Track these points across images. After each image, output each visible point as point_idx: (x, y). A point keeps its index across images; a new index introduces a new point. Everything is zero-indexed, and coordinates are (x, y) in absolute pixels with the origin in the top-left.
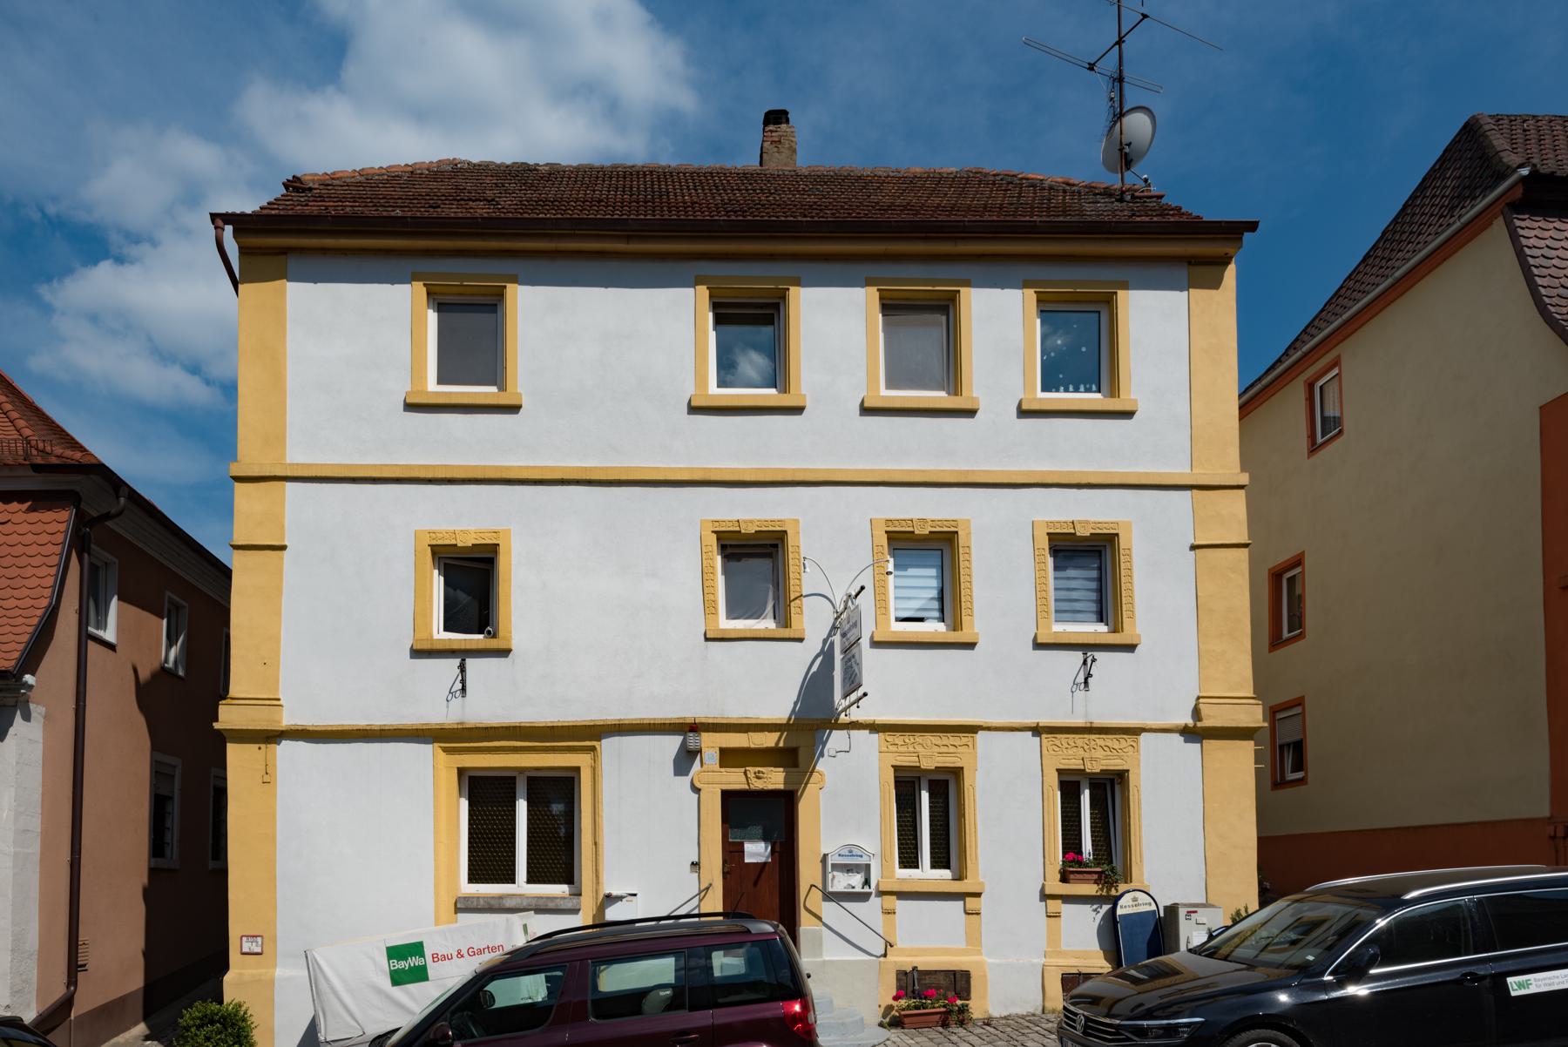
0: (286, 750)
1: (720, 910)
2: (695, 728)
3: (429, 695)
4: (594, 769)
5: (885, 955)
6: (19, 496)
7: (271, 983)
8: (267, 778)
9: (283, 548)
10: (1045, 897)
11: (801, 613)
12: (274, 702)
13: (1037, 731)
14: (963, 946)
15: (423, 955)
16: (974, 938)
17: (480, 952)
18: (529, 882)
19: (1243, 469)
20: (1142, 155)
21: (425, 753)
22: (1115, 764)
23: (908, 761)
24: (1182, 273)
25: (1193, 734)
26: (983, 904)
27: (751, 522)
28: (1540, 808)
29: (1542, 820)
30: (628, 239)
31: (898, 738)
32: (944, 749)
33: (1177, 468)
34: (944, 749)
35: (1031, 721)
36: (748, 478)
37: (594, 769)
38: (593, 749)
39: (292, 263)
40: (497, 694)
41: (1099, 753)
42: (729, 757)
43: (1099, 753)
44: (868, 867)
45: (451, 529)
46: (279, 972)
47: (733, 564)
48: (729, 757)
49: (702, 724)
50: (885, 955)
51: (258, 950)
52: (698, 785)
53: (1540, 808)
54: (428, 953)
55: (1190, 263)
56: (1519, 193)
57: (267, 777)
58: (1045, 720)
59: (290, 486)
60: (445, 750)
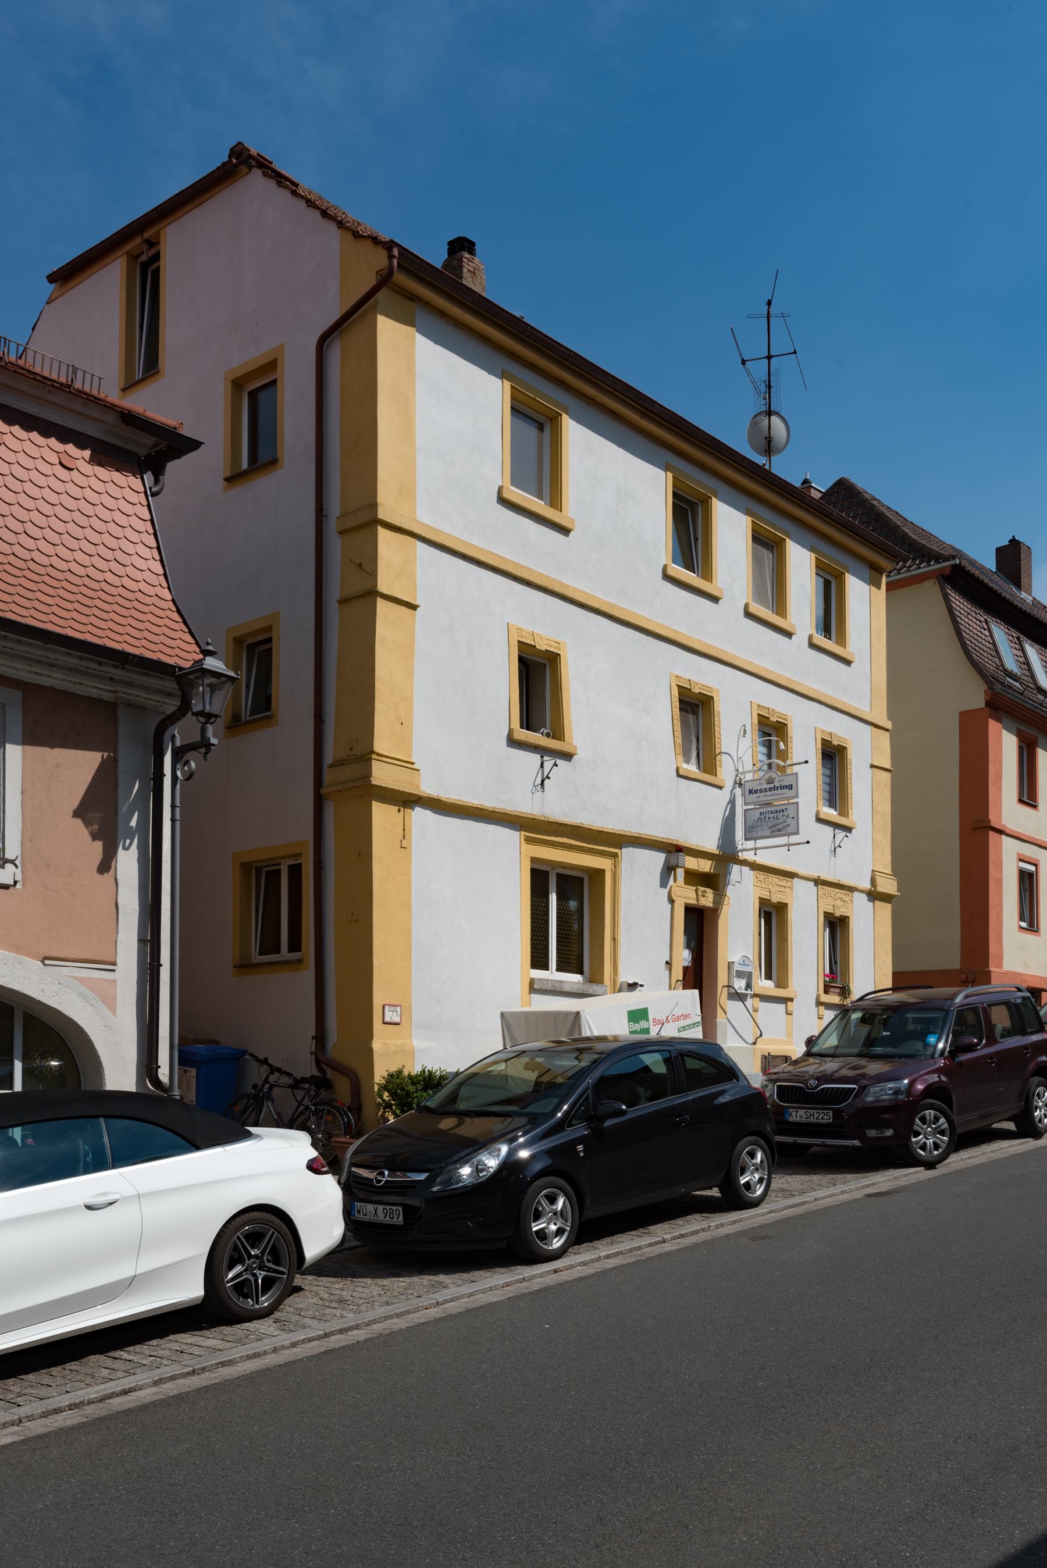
0: (419, 815)
1: (890, 986)
2: (679, 849)
4: (614, 874)
5: (755, 1043)
6: (81, 441)
10: (819, 1003)
13: (818, 882)
14: (784, 1038)
15: (648, 1020)
17: (678, 1019)
18: (558, 970)
19: (889, 719)
20: (780, 451)
21: (512, 838)
23: (765, 895)
24: (866, 571)
28: (956, 964)
29: (955, 970)
30: (643, 415)
31: (762, 876)
32: (780, 889)
35: (815, 874)
36: (696, 647)
37: (614, 874)
38: (615, 856)
39: (420, 314)
41: (839, 903)
45: (531, 630)
49: (686, 848)
50: (755, 1043)
51: (397, 1020)
53: (956, 964)
54: (651, 1018)
55: (871, 567)
56: (947, 572)
58: (825, 876)
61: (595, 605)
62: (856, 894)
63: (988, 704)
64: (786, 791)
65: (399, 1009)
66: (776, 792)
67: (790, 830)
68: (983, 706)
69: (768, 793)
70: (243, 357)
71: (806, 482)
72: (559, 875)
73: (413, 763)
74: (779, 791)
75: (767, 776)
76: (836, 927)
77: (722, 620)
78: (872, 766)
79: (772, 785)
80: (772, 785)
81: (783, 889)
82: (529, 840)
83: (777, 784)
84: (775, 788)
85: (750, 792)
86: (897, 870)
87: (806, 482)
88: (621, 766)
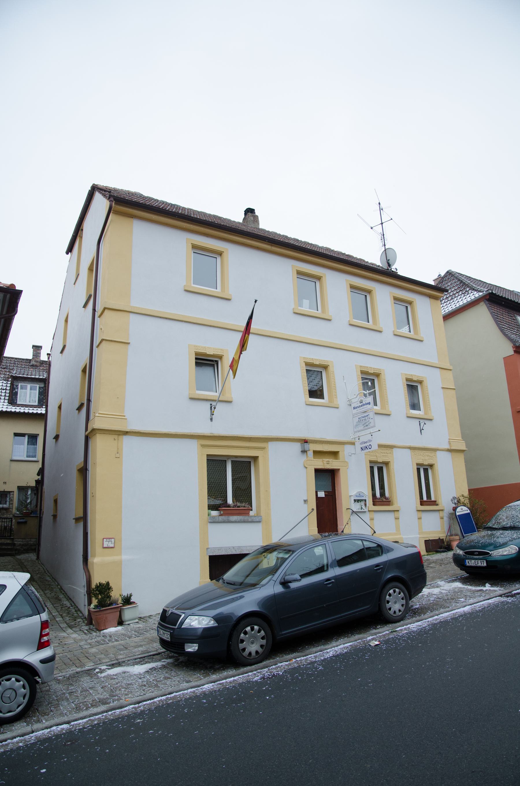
2: (306, 441)
3: (198, 421)
7: (119, 564)
8: (118, 455)
9: (129, 343)
11: (336, 398)
12: (123, 418)
13: (410, 448)
16: (398, 528)
21: (194, 444)
22: (430, 462)
25: (450, 451)
26: (400, 515)
27: (317, 360)
32: (384, 454)
33: (435, 361)
34: (384, 454)
40: (226, 423)
41: (427, 458)
42: (317, 453)
43: (427, 458)
44: (365, 500)
46: (124, 557)
47: (199, 368)
48: (317, 453)
51: (112, 545)
52: (307, 466)
57: (118, 455)
59: (132, 316)
60: (379, 549)
61: (337, 347)
62: (438, 453)
63: (515, 351)
64: (368, 405)
65: (113, 540)
66: (364, 407)
67: (371, 425)
68: (513, 353)
69: (361, 408)
70: (392, 334)
71: (249, 211)
72: (232, 462)
73: (125, 416)
74: (365, 406)
75: (360, 400)
76: (424, 471)
77: (386, 342)
78: (443, 388)
79: (362, 404)
80: (362, 404)
81: (386, 455)
82: (203, 446)
83: (364, 403)
84: (364, 405)
85: (354, 408)
86: (464, 437)
87: (249, 211)
88: (264, 403)
